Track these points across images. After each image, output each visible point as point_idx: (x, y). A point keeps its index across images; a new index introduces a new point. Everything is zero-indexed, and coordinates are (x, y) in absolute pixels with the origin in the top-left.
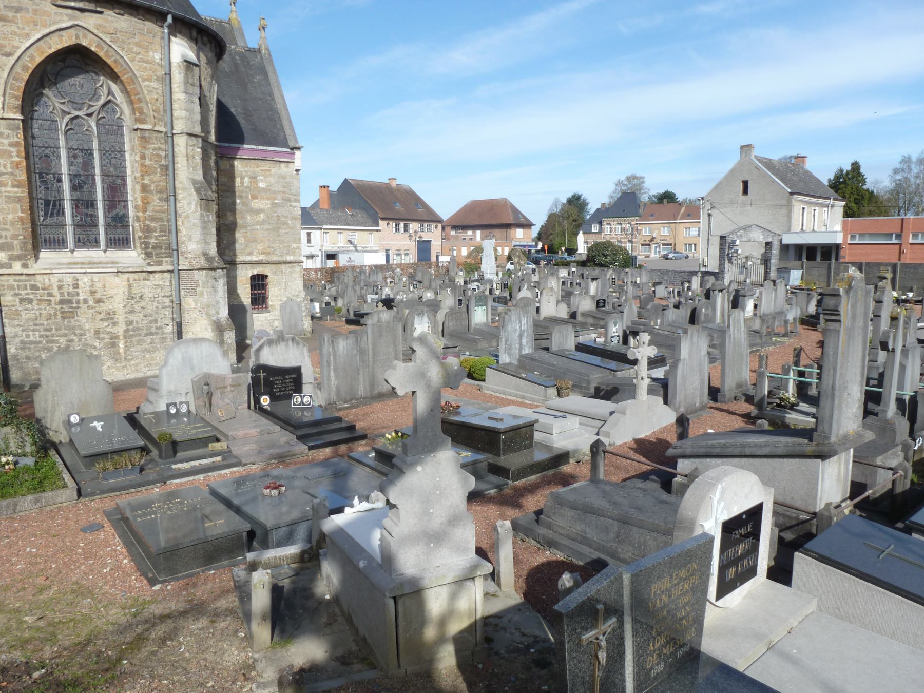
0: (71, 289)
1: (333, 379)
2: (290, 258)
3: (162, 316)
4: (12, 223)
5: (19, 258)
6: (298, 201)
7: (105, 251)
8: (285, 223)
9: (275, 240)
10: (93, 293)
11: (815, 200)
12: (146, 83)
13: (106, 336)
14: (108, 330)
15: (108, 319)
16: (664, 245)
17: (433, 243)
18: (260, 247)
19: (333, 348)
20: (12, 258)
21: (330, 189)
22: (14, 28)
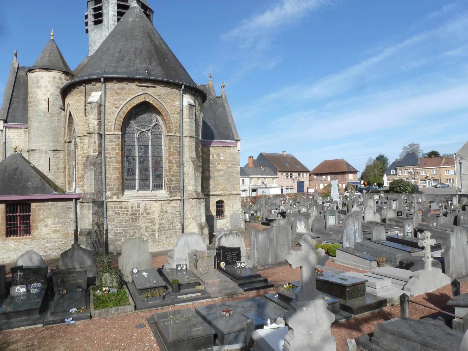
0: (136, 208)
1: (256, 254)
3: (175, 221)
4: (114, 179)
8: (233, 176)
10: (146, 210)
12: (172, 115)
14: (151, 227)
15: (151, 222)
16: (433, 180)
17: (305, 182)
19: (256, 238)
20: (113, 194)
21: (254, 158)
22: (121, 97)
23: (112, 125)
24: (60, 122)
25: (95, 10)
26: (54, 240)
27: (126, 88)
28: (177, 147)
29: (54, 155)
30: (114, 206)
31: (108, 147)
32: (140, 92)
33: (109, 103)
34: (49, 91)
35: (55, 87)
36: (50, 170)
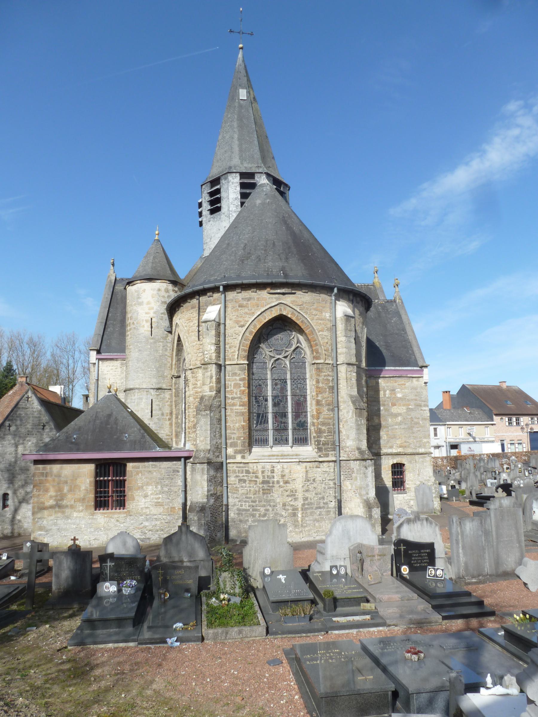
0: (269, 474)
1: (461, 555)
2: (422, 450)
3: (328, 494)
5: (240, 452)
9: (410, 436)
10: (283, 476)
12: (321, 333)
13: (290, 508)
14: (291, 503)
15: (292, 495)
19: (461, 528)
20: (236, 452)
21: (451, 393)
24: (166, 350)
26: (156, 517)
28: (328, 380)
29: (158, 395)
30: (237, 469)
31: (230, 383)
35: (160, 302)
36: (152, 416)
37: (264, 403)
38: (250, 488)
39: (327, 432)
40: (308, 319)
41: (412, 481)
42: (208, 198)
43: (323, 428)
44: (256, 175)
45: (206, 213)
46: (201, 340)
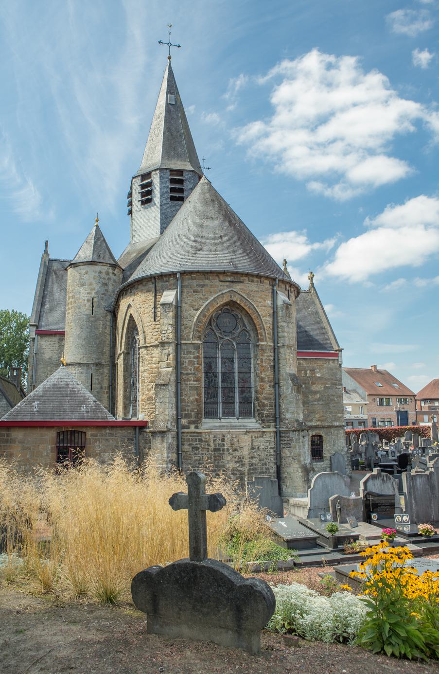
0: (220, 442)
1: (414, 505)
2: (337, 424)
3: (269, 461)
4: (192, 402)
5: (194, 423)
6: (342, 385)
7: (238, 419)
9: (327, 411)
10: (232, 444)
11: (121, 348)
12: (264, 318)
13: (238, 473)
14: (239, 469)
15: (239, 462)
18: (317, 416)
19: (413, 483)
20: (190, 423)
22: (200, 296)
23: (189, 332)
24: (106, 328)
25: (143, 187)
27: (208, 285)
28: (270, 360)
29: (97, 370)
30: (191, 438)
31: (184, 360)
32: (225, 289)
33: (186, 303)
34: (94, 289)
35: (101, 283)
36: (91, 390)
37: (214, 379)
38: (203, 455)
39: (269, 405)
40: (254, 305)
41: (328, 451)
42: (139, 189)
43: (266, 402)
44: (184, 172)
45: (137, 204)
46: (158, 319)
